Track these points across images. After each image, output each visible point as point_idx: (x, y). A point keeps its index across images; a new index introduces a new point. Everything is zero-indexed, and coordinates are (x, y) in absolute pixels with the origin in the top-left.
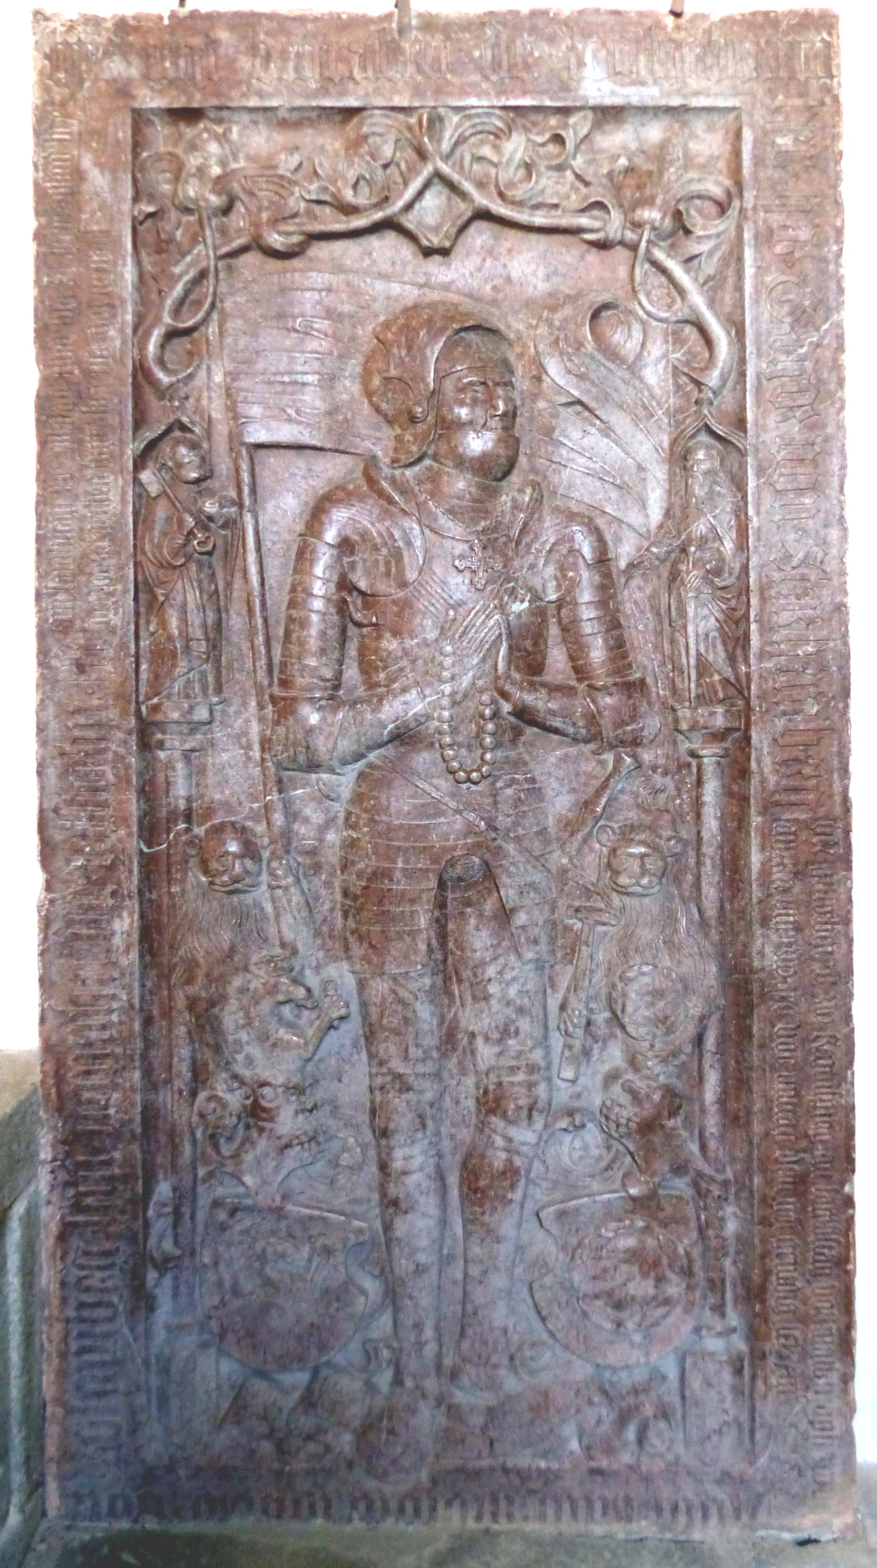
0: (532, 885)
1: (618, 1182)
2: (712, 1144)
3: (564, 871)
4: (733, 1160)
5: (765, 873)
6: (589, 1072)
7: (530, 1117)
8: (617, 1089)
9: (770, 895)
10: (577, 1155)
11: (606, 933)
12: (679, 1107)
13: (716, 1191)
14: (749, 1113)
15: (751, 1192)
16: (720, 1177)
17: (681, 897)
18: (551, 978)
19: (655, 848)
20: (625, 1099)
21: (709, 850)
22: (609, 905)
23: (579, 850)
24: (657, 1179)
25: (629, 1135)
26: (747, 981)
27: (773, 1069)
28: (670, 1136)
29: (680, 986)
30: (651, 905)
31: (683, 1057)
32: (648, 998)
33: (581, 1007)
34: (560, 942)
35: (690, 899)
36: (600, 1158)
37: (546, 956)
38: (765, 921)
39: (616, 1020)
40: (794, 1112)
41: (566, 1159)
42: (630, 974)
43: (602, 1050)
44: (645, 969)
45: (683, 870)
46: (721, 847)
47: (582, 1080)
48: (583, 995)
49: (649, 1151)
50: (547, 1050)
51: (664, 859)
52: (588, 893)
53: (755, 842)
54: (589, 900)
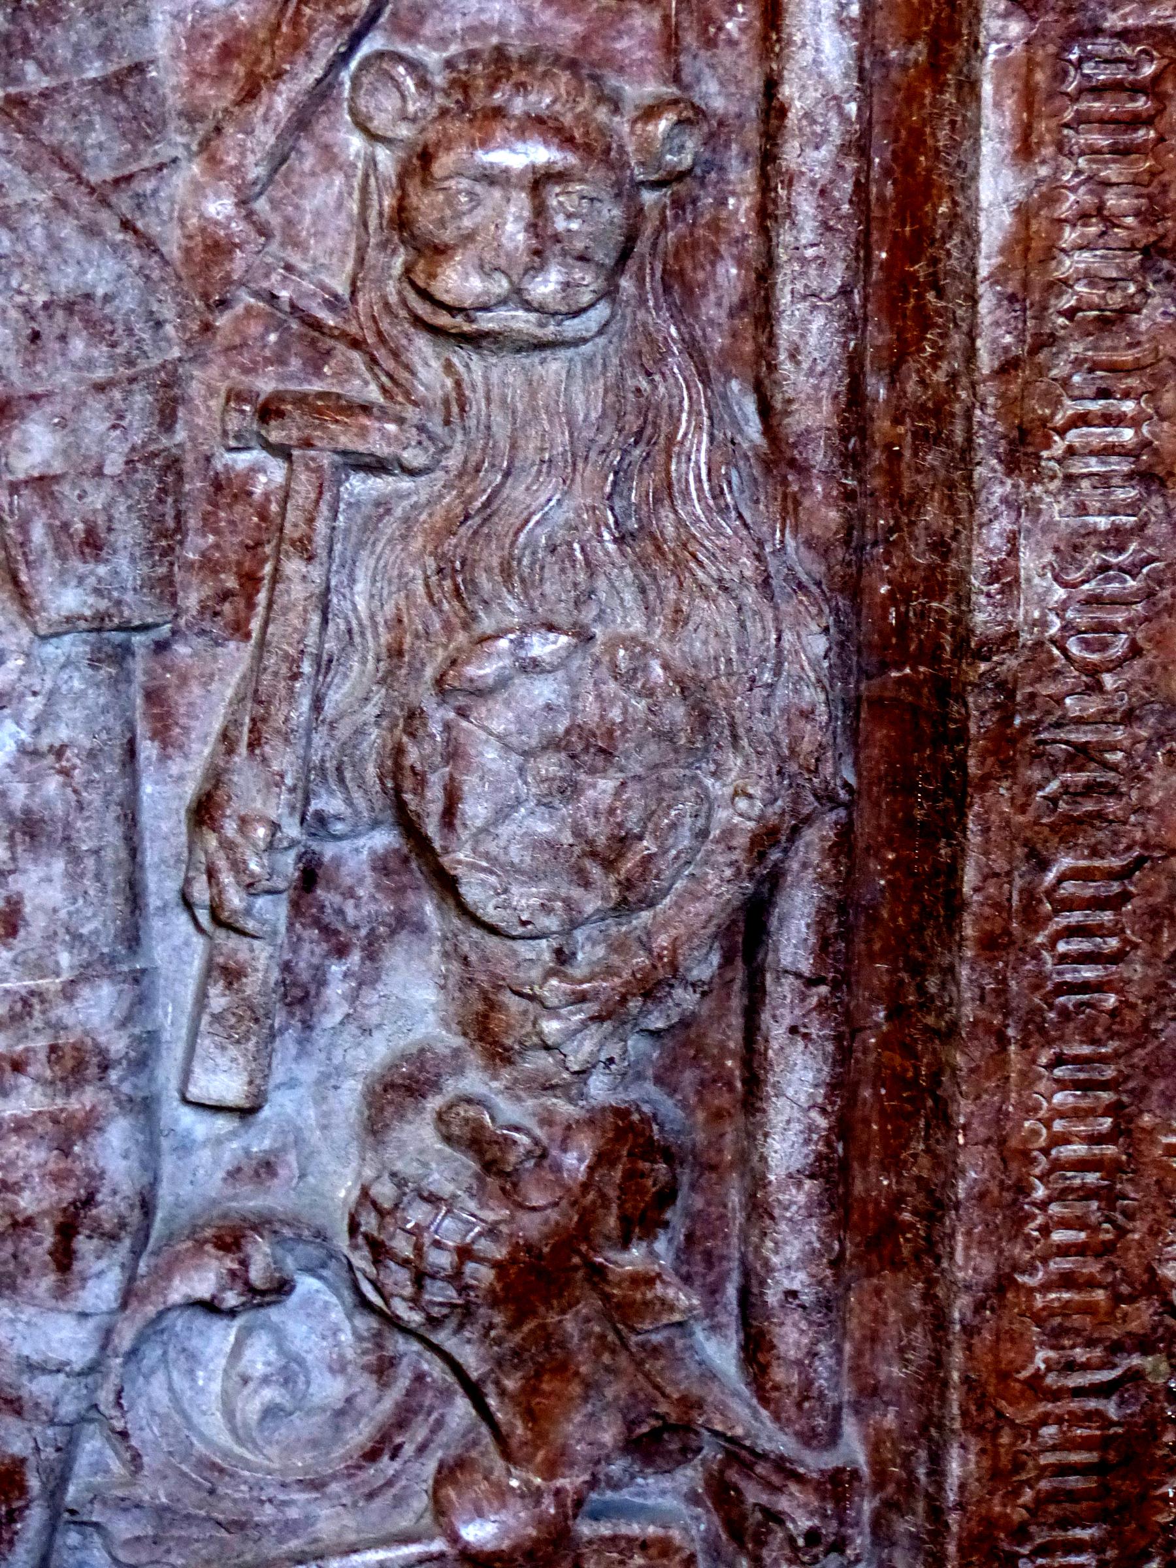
0: (78, 306)
1: (421, 1502)
2: (791, 1336)
3: (215, 248)
4: (870, 1392)
5: (1031, 247)
6: (308, 1072)
7: (64, 1258)
8: (418, 1136)
9: (1046, 341)
10: (252, 1406)
11: (383, 506)
12: (667, 1196)
13: (800, 1513)
14: (937, 1206)
15: (936, 1513)
16: (815, 1462)
17: (693, 348)
18: (153, 696)
19: (595, 148)
20: (447, 1172)
21: (812, 159)
22: (397, 387)
23: (279, 160)
24: (569, 1482)
25: (465, 1313)
26: (948, 689)
27: (1036, 1031)
28: (626, 1308)
29: (677, 712)
30: (571, 387)
31: (686, 998)
32: (550, 765)
33: (277, 807)
34: (194, 546)
35: (728, 355)
36: (345, 1411)
37: (137, 609)
38: (1022, 449)
39: (422, 860)
40: (1108, 1196)
41: (214, 1426)
42: (484, 670)
43: (364, 981)
44: (542, 647)
45: (699, 248)
46: (859, 146)
47: (281, 1105)
48: (284, 760)
49: (542, 1370)
50: (141, 988)
51: (626, 192)
52: (313, 338)
53: (995, 119)
54: (319, 371)
